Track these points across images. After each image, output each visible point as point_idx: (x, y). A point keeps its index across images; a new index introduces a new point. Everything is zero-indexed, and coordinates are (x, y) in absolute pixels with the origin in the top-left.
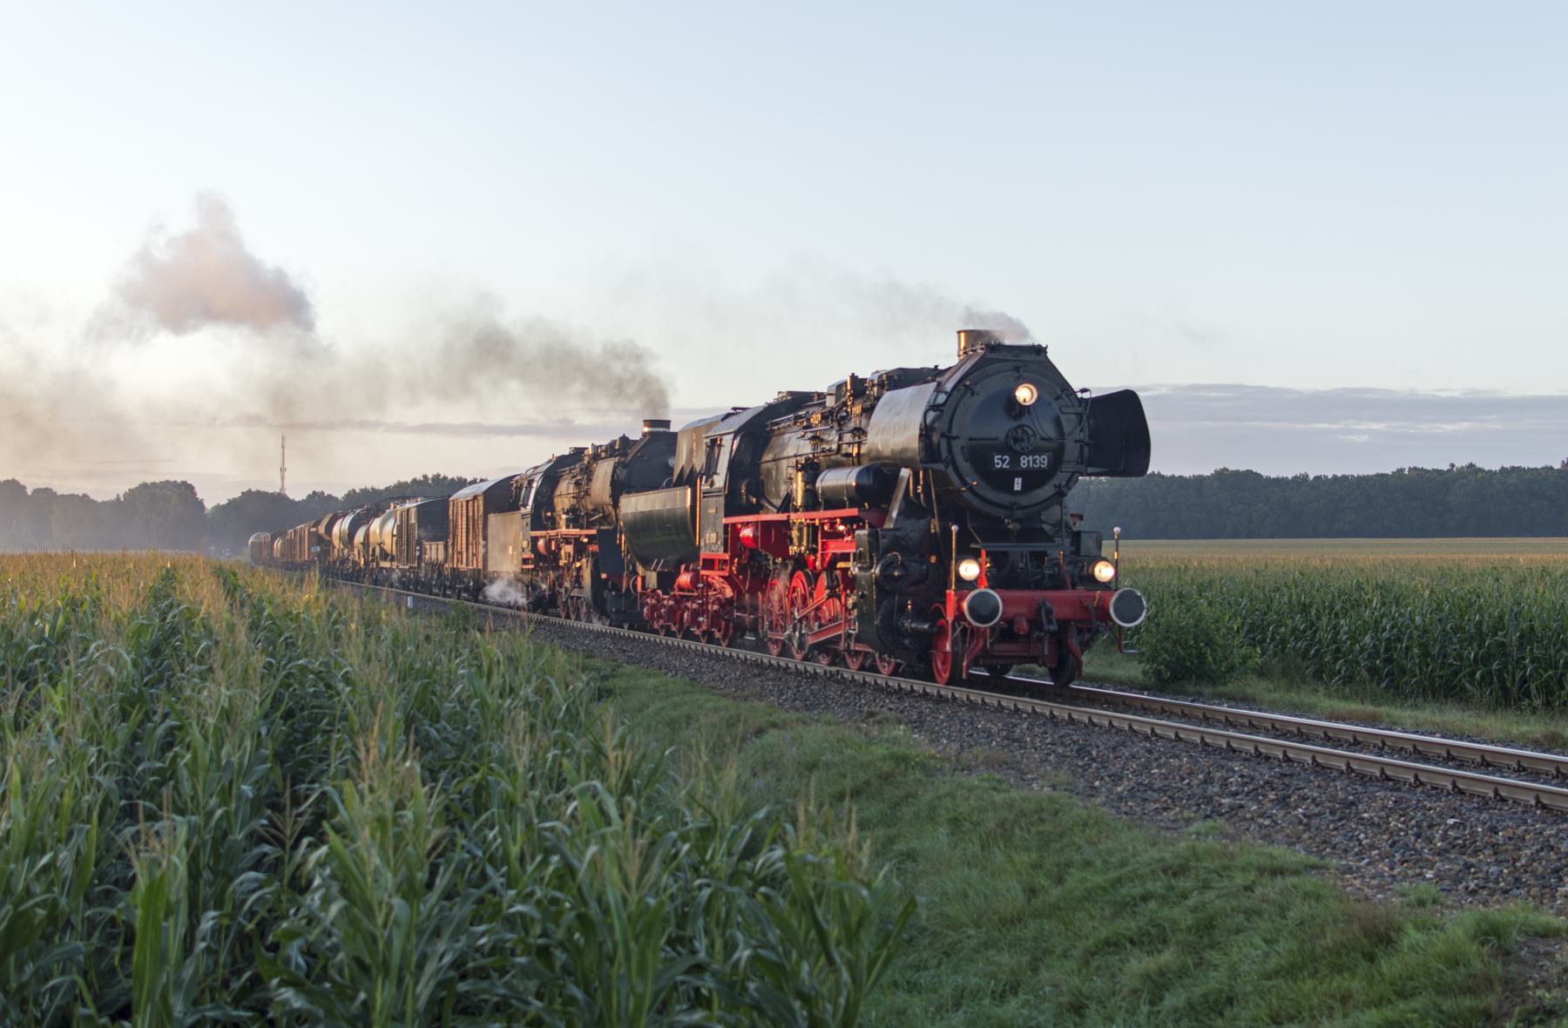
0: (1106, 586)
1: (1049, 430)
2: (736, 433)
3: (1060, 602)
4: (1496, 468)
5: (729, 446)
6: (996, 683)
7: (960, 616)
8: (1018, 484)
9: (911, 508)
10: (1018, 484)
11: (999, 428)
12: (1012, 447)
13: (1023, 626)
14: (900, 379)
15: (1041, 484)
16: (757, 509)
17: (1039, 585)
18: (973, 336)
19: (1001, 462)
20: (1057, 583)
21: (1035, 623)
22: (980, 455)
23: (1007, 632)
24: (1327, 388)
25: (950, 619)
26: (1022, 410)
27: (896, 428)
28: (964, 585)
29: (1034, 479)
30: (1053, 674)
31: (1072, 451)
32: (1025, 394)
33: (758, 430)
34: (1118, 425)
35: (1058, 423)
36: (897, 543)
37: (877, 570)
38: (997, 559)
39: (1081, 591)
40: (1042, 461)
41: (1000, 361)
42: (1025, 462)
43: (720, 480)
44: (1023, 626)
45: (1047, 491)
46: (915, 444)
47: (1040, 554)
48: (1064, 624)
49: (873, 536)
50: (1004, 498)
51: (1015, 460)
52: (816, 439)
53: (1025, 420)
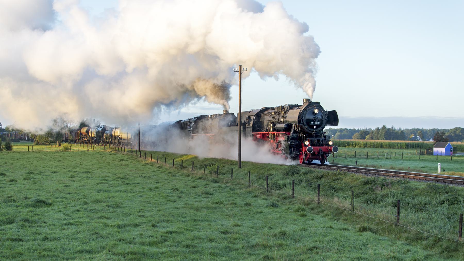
0: (331, 146)
1: (320, 117)
2: (254, 116)
3: (323, 148)
4: (429, 129)
5: (253, 118)
6: (310, 163)
7: (306, 151)
8: (315, 127)
9: (295, 132)
10: (315, 127)
11: (312, 117)
12: (313, 121)
13: (316, 153)
14: (292, 107)
15: (319, 127)
16: (261, 131)
17: (319, 146)
18: (264, 79)
19: (312, 123)
20: (322, 145)
21: (319, 152)
22: (308, 122)
23: (314, 154)
24: (261, 162)
25: (303, 152)
26: (316, 114)
27: (293, 116)
28: (305, 145)
29: (318, 126)
30: (321, 162)
31: (324, 121)
32: (316, 111)
33: (260, 114)
34: (332, 118)
35: (322, 116)
36: (293, 138)
37: (289, 143)
38: (311, 141)
39: (326, 146)
40: (319, 123)
41: (311, 105)
42: (316, 123)
43: (251, 124)
44: (316, 153)
45: (320, 128)
46: (297, 120)
47: (320, 140)
48: (324, 152)
49: (288, 137)
50: (312, 130)
51: (314, 123)
52: (273, 118)
53: (316, 116)
